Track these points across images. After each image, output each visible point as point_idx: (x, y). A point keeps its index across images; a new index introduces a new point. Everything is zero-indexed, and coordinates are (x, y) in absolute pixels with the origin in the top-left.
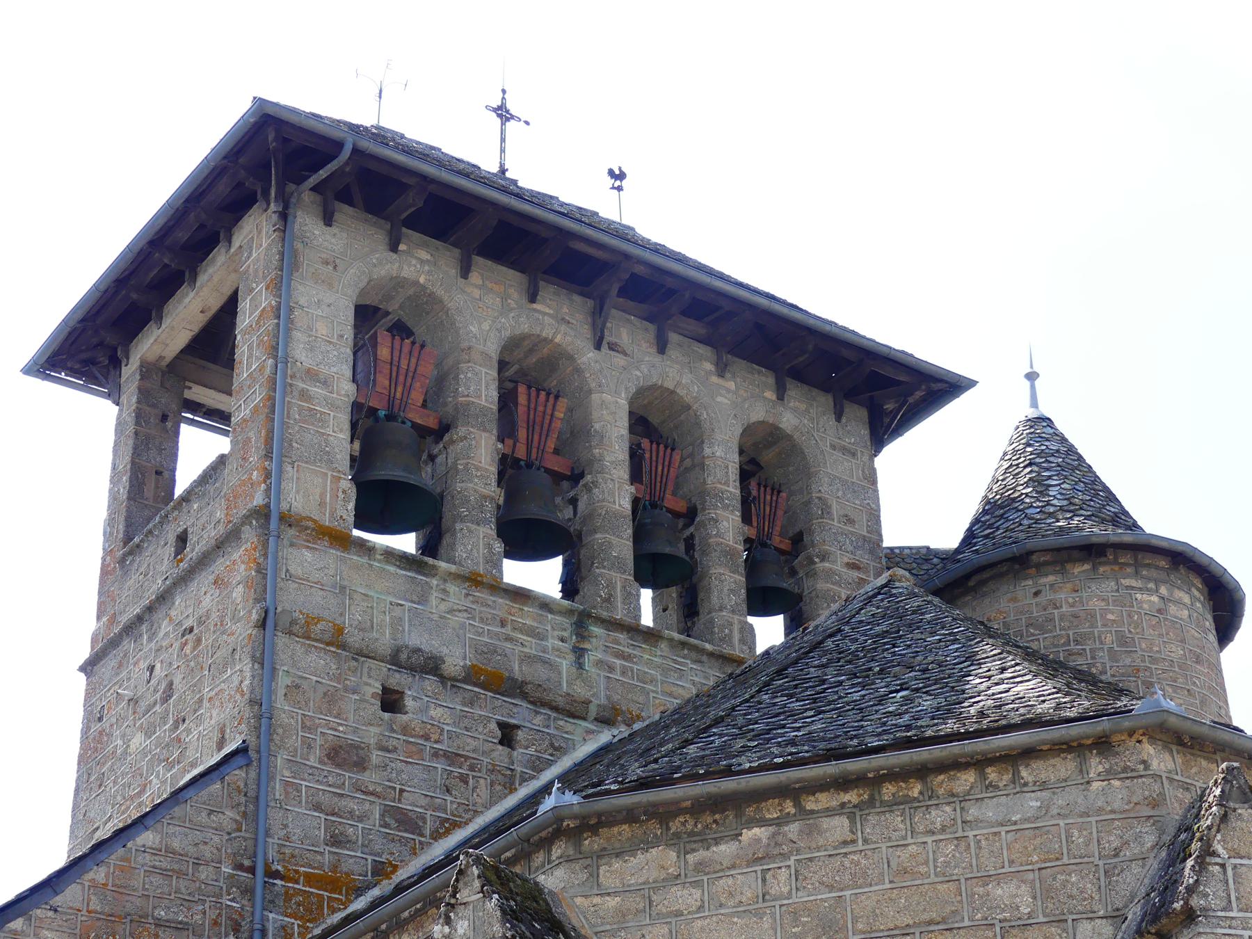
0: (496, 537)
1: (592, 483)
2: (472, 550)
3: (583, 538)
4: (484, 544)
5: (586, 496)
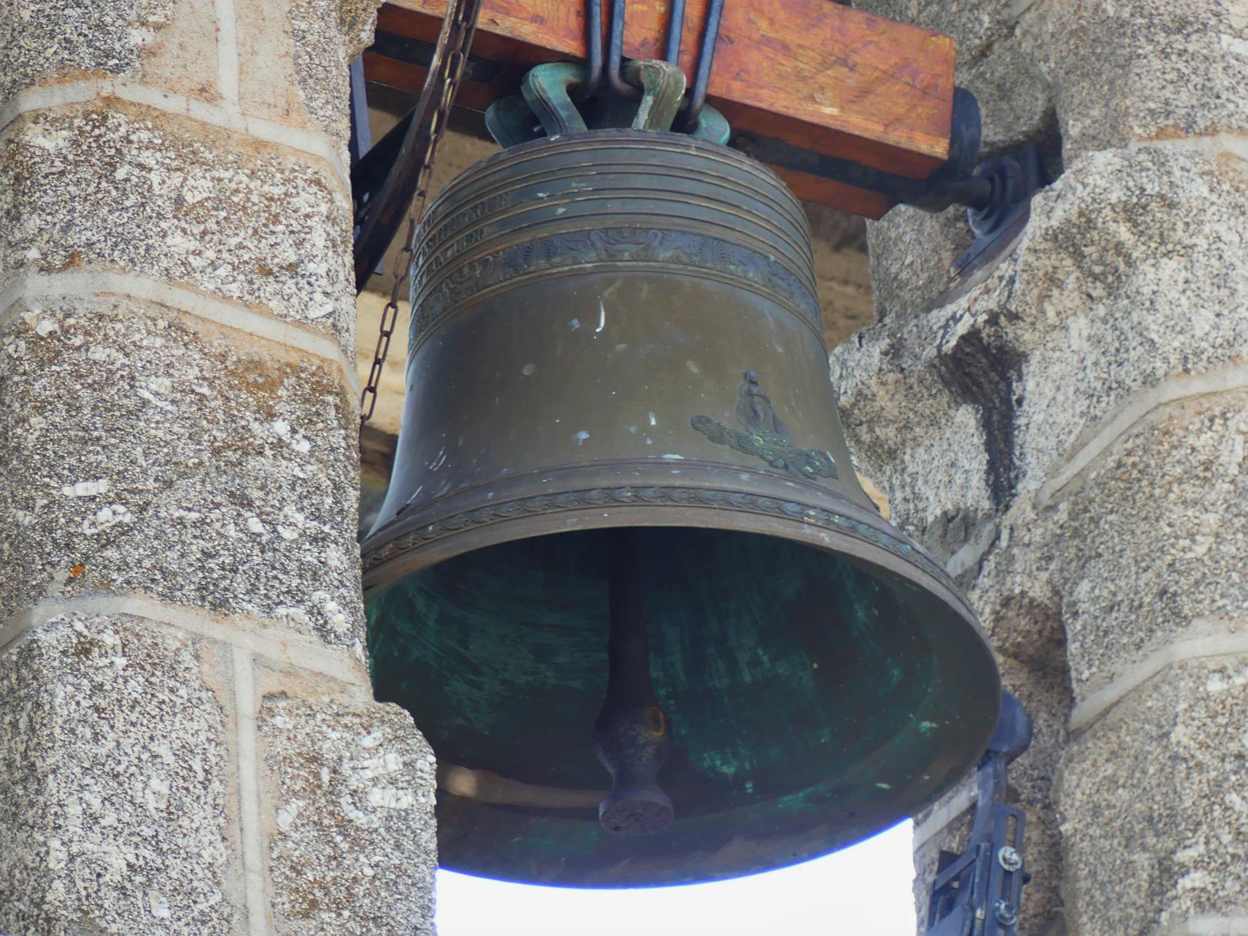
0: (361, 694)
1: (1131, 212)
2: (172, 813)
3: (1081, 670)
4: (272, 762)
5: (1080, 326)
